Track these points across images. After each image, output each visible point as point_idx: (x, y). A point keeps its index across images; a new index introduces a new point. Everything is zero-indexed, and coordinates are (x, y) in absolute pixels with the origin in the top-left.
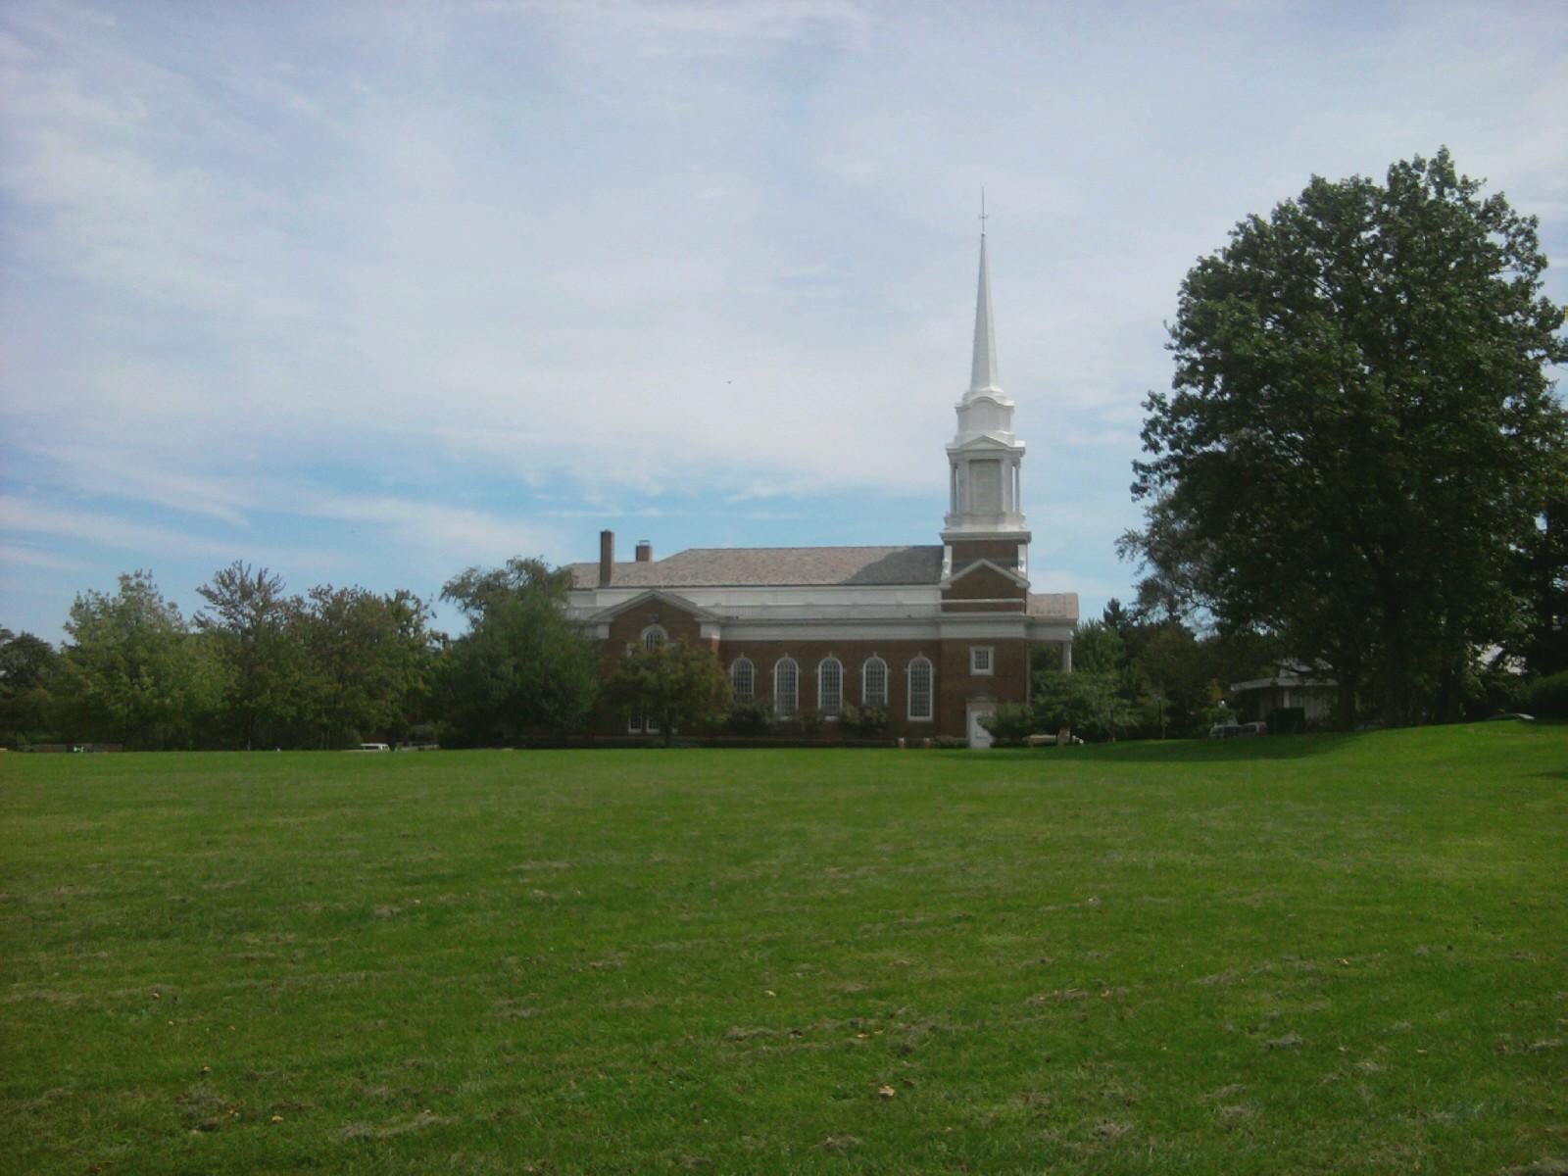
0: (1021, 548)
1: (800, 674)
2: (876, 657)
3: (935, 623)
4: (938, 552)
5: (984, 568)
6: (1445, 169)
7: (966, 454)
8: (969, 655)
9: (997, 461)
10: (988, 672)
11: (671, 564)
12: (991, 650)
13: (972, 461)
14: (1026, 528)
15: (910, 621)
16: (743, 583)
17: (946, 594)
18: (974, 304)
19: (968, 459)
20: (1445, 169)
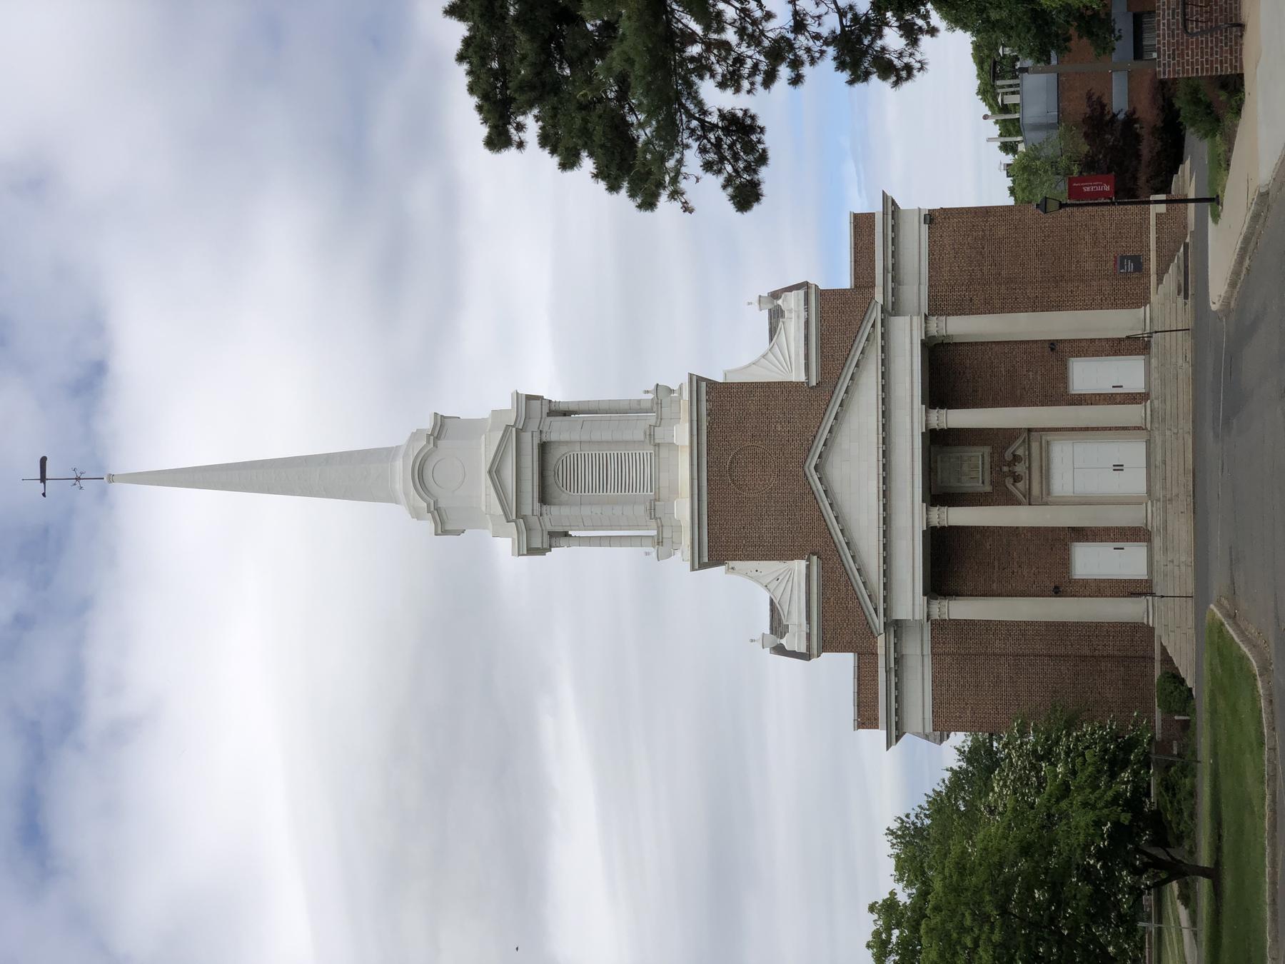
7: (527, 510)
9: (544, 448)
13: (544, 498)
19: (537, 505)
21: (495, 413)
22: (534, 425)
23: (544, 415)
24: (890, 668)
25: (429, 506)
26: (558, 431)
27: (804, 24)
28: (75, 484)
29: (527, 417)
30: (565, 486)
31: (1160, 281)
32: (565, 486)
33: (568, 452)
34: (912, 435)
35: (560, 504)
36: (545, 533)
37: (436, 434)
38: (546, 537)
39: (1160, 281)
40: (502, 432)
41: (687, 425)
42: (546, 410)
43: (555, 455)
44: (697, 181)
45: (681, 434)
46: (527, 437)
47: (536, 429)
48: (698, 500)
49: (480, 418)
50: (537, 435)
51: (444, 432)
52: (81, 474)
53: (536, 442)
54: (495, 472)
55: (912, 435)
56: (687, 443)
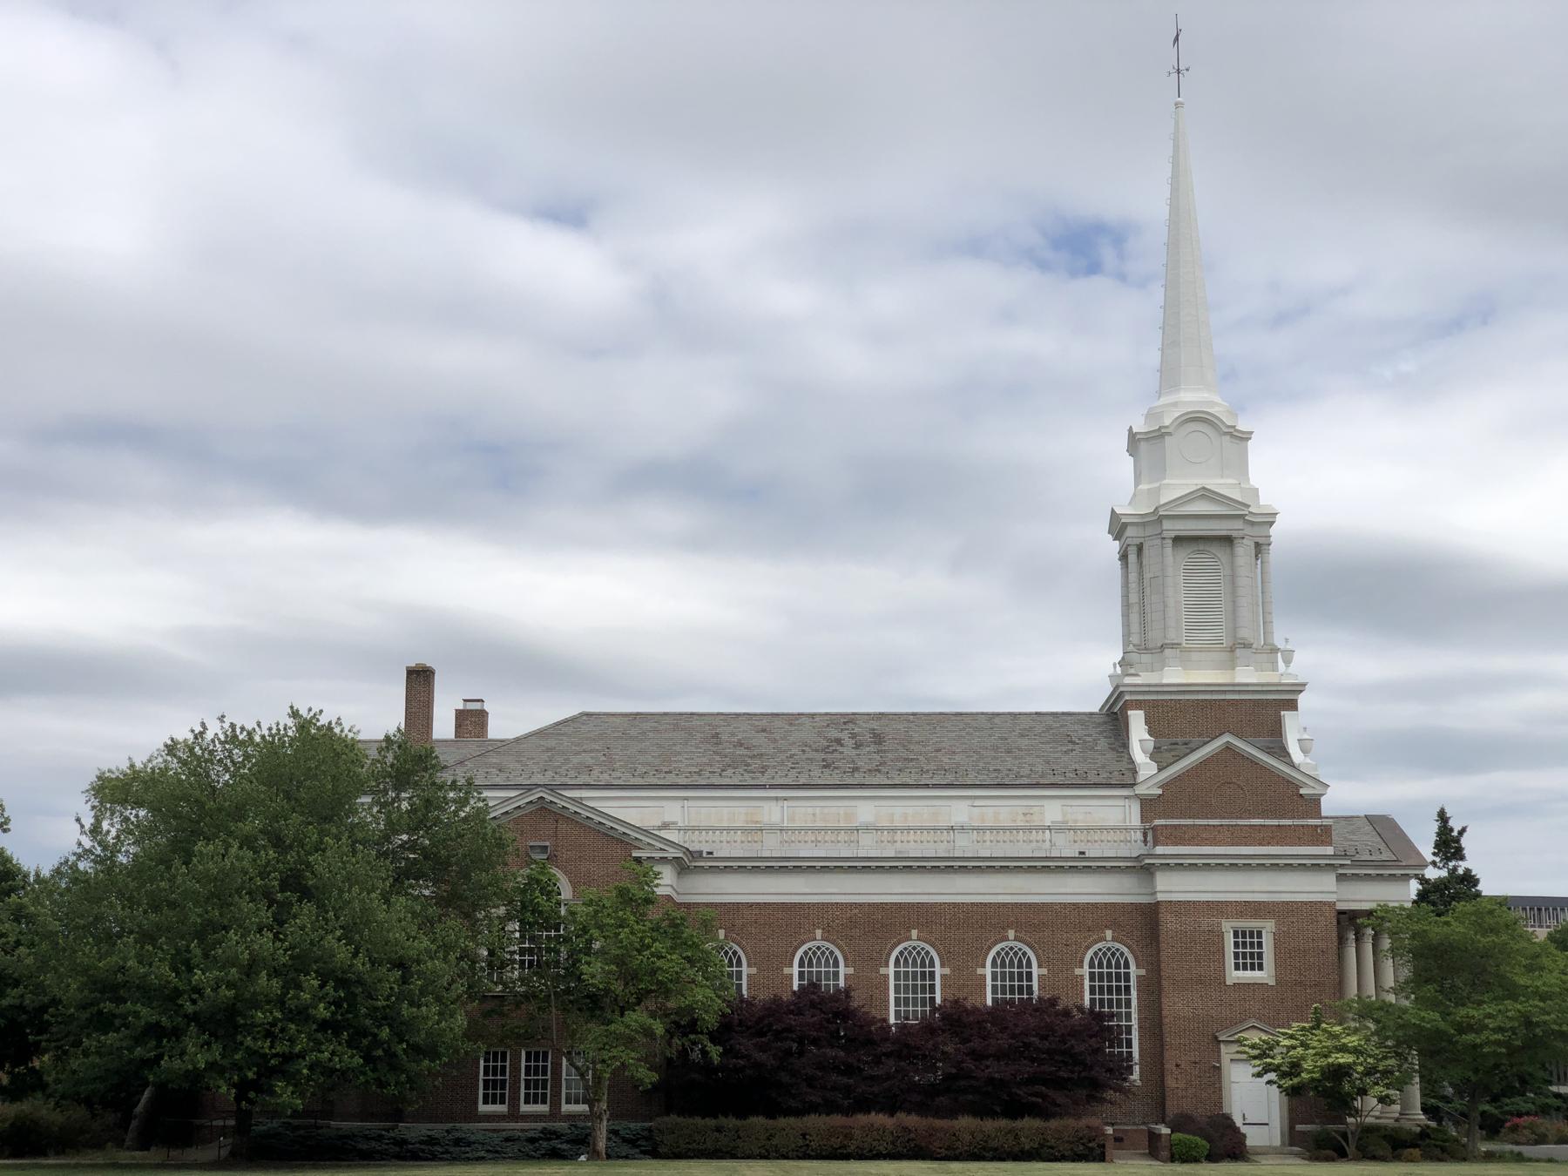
0: (1287, 716)
1: (1150, 483)
2: (1011, 941)
3: (1144, 869)
4: (1318, 815)
5: (1228, 748)
6: (469, 1041)
7: (1167, 525)
8: (1221, 935)
9: (1228, 541)
10: (1265, 976)
11: (552, 743)
12: (1268, 928)
13: (1179, 540)
14: (1284, 674)
15: (1081, 865)
16: (716, 780)
17: (1149, 806)
18: (1166, 191)
19: (1173, 534)
20: (469, 1041)
21: (1255, 492)
22: (1248, 530)
23: (1257, 540)
24: (1143, 860)
25: (1167, 427)
26: (1244, 551)
27: (834, 993)
28: (1174, 68)
29: (1253, 524)
30: (1190, 560)
31: (1348, 1144)
32: (1190, 560)
33: (1222, 564)
34: (1253, 892)
35: (1174, 555)
36: (1142, 540)
37: (1235, 434)
38: (1138, 541)
39: (1348, 1144)
40: (1240, 500)
41: (1254, 681)
42: (1261, 541)
43: (1220, 552)
44: (223, 716)
45: (1247, 675)
46: (1238, 524)
47: (1245, 532)
48: (1212, 691)
49: (1250, 475)
50: (1241, 533)
51: (1237, 441)
52: (1174, 68)
53: (1234, 534)
54: (1205, 494)
55: (1253, 892)
56: (1165, 681)
